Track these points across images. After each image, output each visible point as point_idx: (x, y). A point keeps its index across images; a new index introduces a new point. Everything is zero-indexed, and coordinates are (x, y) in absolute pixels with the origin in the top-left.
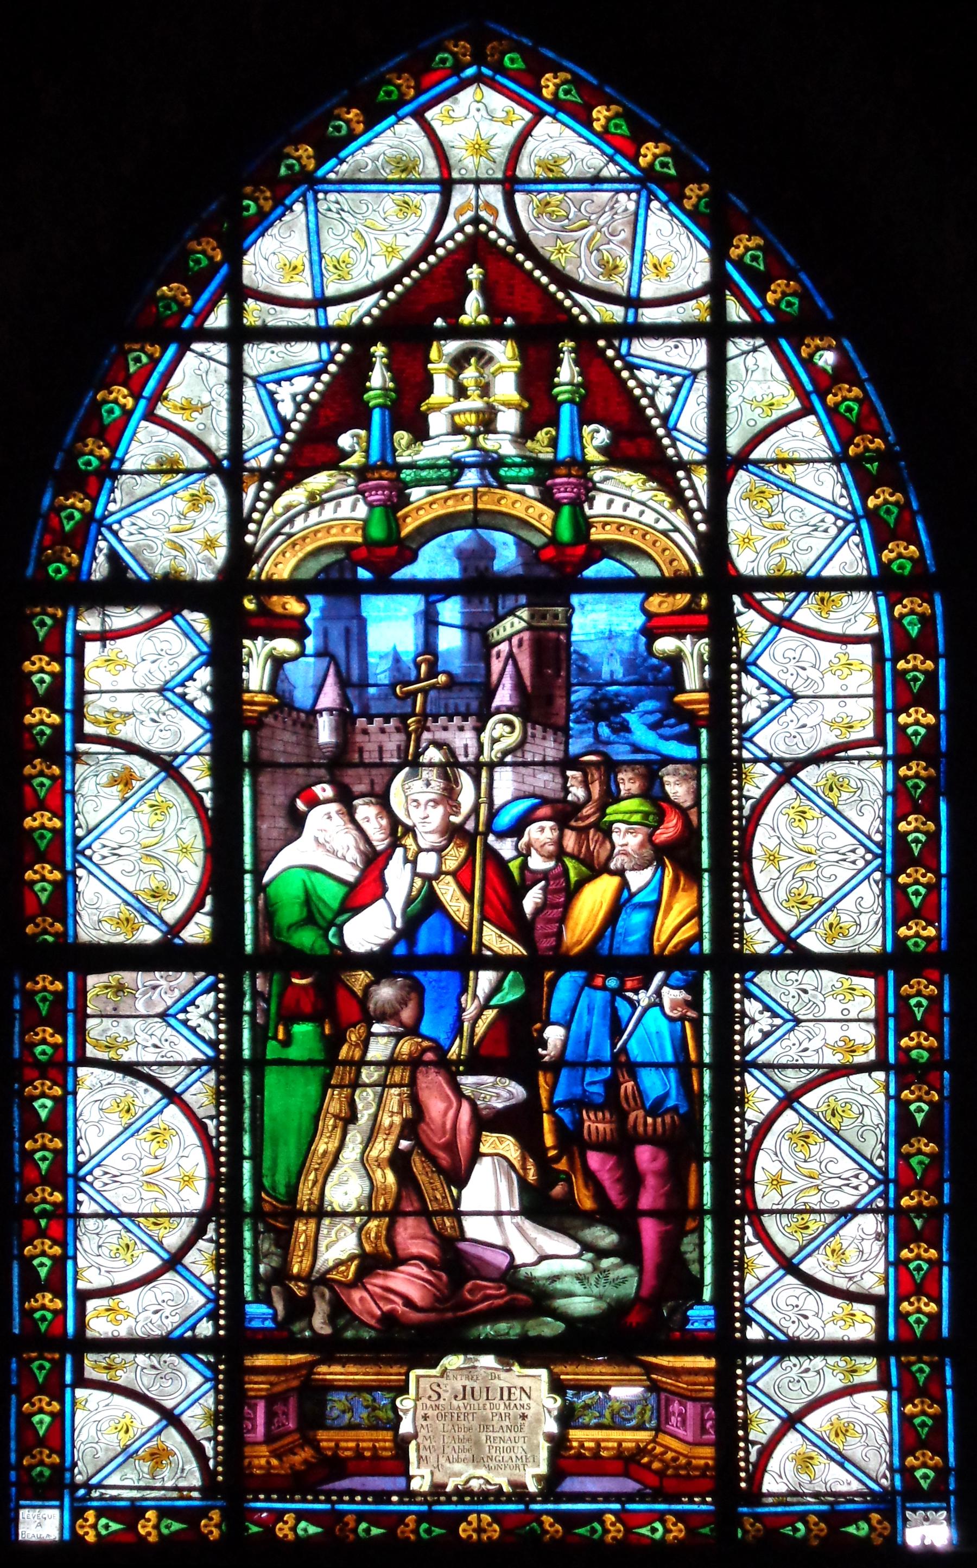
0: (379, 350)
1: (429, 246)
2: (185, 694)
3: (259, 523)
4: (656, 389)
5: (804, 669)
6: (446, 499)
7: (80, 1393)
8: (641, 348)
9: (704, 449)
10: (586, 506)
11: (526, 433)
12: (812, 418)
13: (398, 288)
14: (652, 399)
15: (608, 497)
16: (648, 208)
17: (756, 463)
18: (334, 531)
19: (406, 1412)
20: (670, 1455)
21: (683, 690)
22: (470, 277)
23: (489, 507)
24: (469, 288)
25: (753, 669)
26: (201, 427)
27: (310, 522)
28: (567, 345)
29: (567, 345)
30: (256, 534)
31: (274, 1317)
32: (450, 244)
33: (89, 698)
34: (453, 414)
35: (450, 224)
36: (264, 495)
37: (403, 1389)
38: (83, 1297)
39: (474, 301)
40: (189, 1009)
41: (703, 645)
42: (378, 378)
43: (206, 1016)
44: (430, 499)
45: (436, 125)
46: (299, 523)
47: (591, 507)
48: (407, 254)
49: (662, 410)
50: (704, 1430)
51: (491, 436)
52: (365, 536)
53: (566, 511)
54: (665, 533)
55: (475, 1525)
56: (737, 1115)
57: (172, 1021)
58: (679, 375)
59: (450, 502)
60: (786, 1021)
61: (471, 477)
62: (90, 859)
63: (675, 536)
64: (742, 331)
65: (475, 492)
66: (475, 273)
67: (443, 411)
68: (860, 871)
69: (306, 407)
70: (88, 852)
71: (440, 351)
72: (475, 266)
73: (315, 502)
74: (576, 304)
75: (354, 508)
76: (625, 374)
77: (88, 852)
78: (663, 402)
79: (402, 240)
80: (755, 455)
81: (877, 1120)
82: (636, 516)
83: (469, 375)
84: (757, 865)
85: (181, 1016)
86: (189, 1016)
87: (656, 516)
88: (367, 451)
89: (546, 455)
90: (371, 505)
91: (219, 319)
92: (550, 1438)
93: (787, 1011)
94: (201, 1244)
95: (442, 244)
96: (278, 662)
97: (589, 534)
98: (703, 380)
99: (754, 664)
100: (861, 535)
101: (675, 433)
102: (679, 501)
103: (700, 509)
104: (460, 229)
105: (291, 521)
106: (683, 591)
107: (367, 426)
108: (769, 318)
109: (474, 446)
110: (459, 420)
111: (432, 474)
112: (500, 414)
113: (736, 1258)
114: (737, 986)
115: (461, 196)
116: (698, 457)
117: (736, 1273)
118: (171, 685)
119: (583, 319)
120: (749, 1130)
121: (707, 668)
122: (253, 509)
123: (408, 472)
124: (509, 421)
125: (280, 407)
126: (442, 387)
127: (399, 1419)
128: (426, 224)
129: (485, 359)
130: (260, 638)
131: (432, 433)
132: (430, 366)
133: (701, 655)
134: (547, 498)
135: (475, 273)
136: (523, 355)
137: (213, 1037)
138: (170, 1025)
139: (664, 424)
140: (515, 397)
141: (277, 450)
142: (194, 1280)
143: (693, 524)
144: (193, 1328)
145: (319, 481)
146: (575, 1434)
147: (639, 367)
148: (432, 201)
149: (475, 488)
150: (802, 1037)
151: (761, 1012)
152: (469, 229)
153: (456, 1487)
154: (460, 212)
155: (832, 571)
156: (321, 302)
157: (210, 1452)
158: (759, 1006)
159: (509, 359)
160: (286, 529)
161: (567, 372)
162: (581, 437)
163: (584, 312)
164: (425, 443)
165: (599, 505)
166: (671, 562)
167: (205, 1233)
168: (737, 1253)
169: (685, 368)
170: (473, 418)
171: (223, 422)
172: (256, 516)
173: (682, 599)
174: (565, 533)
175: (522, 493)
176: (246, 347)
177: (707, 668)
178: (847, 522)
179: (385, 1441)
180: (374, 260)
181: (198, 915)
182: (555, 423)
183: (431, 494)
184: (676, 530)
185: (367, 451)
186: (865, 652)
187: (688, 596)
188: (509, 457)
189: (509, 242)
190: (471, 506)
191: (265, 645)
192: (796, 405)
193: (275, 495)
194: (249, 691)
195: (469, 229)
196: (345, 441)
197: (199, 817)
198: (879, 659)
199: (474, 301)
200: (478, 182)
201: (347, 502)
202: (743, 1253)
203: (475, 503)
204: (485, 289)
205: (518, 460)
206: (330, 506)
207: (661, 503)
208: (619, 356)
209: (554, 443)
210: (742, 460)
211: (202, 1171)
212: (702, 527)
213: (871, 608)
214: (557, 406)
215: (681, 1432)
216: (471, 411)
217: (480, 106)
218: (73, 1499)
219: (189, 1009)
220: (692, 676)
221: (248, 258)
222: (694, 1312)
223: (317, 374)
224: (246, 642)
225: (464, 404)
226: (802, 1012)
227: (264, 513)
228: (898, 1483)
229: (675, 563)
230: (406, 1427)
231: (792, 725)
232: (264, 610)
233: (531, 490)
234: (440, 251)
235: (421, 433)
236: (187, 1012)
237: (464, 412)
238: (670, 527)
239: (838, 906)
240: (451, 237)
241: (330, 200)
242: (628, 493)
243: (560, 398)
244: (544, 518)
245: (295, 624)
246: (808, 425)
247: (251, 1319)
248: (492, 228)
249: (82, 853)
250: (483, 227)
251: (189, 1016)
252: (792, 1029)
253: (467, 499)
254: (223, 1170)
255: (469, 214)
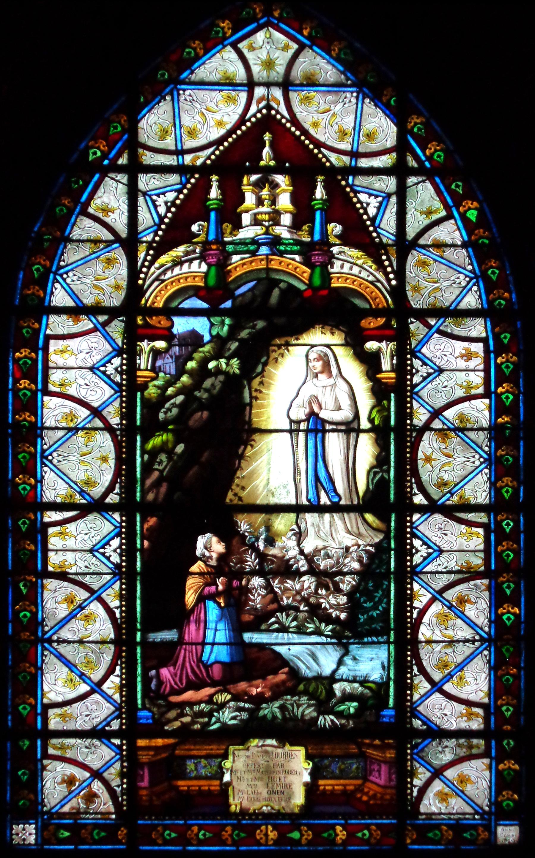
0: (214, 178)
1: (242, 121)
2: (105, 553)
3: (146, 274)
4: (368, 204)
5: (446, 356)
6: (251, 262)
7: (45, 762)
8: (360, 181)
9: (393, 238)
10: (329, 267)
11: (296, 226)
12: (452, 221)
13: (226, 144)
14: (365, 210)
15: (341, 262)
16: (363, 102)
17: (424, 247)
18: (189, 280)
19: (227, 770)
20: (371, 793)
21: (381, 371)
22: (265, 138)
23: (274, 267)
24: (264, 146)
25: (418, 354)
26: (113, 220)
27: (174, 274)
28: (320, 178)
29: (320, 178)
30: (144, 280)
31: (153, 718)
32: (253, 120)
33: (51, 372)
34: (255, 215)
35: (253, 109)
36: (149, 258)
37: (225, 756)
38: (47, 707)
39: (266, 152)
40: (107, 365)
41: (392, 345)
42: (214, 193)
43: (115, 551)
44: (241, 262)
45: (245, 51)
46: (169, 274)
47: (332, 267)
48: (229, 127)
49: (371, 216)
50: (391, 780)
51: (277, 227)
52: (206, 282)
53: (318, 270)
54: (372, 283)
55: (264, 832)
56: (408, 606)
57: (97, 554)
58: (381, 196)
59: (253, 264)
60: (435, 551)
61: (264, 250)
62: (51, 462)
63: (379, 284)
64: (414, 172)
65: (267, 258)
66: (267, 137)
67: (250, 212)
68: (477, 467)
69: (173, 209)
70: (50, 458)
71: (248, 180)
72: (267, 133)
73: (178, 262)
74: (324, 156)
75: (200, 266)
76: (352, 195)
77: (50, 458)
78: (372, 211)
79: (226, 119)
80: (422, 241)
81: (485, 606)
82: (357, 273)
83: (265, 193)
84: (420, 463)
85: (102, 550)
86: (106, 550)
87: (368, 273)
88: (207, 234)
89: (307, 239)
90: (209, 265)
91: (123, 160)
92: (306, 785)
93: (435, 544)
94: (112, 678)
95: (249, 120)
96: (156, 353)
97: (330, 283)
98: (394, 199)
99: (419, 351)
100: (478, 286)
101: (379, 230)
102: (380, 266)
103: (393, 272)
104: (260, 111)
105: (164, 273)
106: (382, 316)
107: (208, 220)
108: (427, 164)
109: (267, 233)
110: (259, 217)
111: (244, 248)
112: (282, 216)
113: (409, 683)
114: (408, 530)
115: (259, 91)
116: (390, 242)
117: (409, 692)
118: (96, 548)
119: (328, 164)
120: (415, 790)
121: (395, 358)
122: (143, 266)
123: (231, 246)
124: (286, 219)
125: (159, 209)
126: (250, 199)
127: (223, 774)
128: (240, 110)
129: (275, 186)
130: (146, 341)
131: (244, 225)
132: (243, 187)
133: (392, 352)
134: (307, 262)
135: (267, 137)
136: (293, 183)
137: (119, 381)
138: (94, 556)
139: (373, 224)
140: (290, 207)
141: (156, 234)
142: (108, 698)
143: (389, 280)
144: (108, 724)
145: (180, 251)
146: (321, 782)
147: (359, 192)
148: (243, 96)
149: (267, 255)
150: (443, 380)
151: (421, 546)
152: (264, 111)
153: (254, 811)
154: (259, 102)
155: (463, 305)
156: (180, 152)
157: (118, 615)
158: (420, 543)
159: (287, 185)
160: (162, 277)
161: (320, 193)
162: (327, 230)
163: (328, 160)
164: (240, 230)
165: (337, 267)
166: (376, 299)
167: (114, 490)
168: (409, 592)
169: (384, 192)
170: (267, 217)
171: (125, 219)
172: (144, 270)
173: (381, 321)
174: (317, 281)
175: (294, 260)
176: (139, 175)
177: (395, 358)
178: (471, 279)
179: (215, 786)
180: (211, 129)
181: (111, 494)
182: (313, 221)
183: (242, 259)
184: (378, 281)
185: (207, 234)
186: (478, 348)
187: (384, 319)
188: (287, 239)
189: (288, 121)
190: (265, 266)
191: (148, 345)
192: (443, 213)
193: (155, 258)
194: (140, 370)
195: (264, 111)
196: (195, 228)
197: (112, 623)
198: (487, 351)
199: (266, 152)
200: (268, 85)
201: (196, 263)
202: (412, 681)
203: (267, 265)
204: (272, 146)
205: (292, 241)
206: (186, 265)
207: (371, 267)
208: (348, 185)
209: (311, 233)
210: (414, 244)
211: (112, 456)
212: (394, 282)
213: (483, 323)
214: (313, 212)
215: (377, 780)
216: (266, 213)
217: (270, 40)
218: (43, 820)
219: (107, 365)
220: (386, 364)
221: (141, 125)
222: (386, 712)
223: (180, 191)
224: (139, 343)
225: (261, 209)
226: (444, 545)
227: (149, 268)
228: (493, 809)
229: (377, 300)
230: (227, 778)
231: (440, 386)
232: (147, 325)
233: (297, 258)
234: (248, 124)
235: (238, 225)
236: (105, 549)
237: (261, 213)
238: (375, 279)
239: (465, 487)
240: (254, 116)
241: (188, 93)
242: (352, 261)
243: (316, 207)
244: (305, 275)
245: (166, 333)
246: (449, 225)
247: (141, 719)
248: (278, 112)
249: (46, 458)
250: (273, 112)
251: (106, 550)
252: (438, 556)
253: (263, 262)
254: (124, 456)
255: (264, 103)
